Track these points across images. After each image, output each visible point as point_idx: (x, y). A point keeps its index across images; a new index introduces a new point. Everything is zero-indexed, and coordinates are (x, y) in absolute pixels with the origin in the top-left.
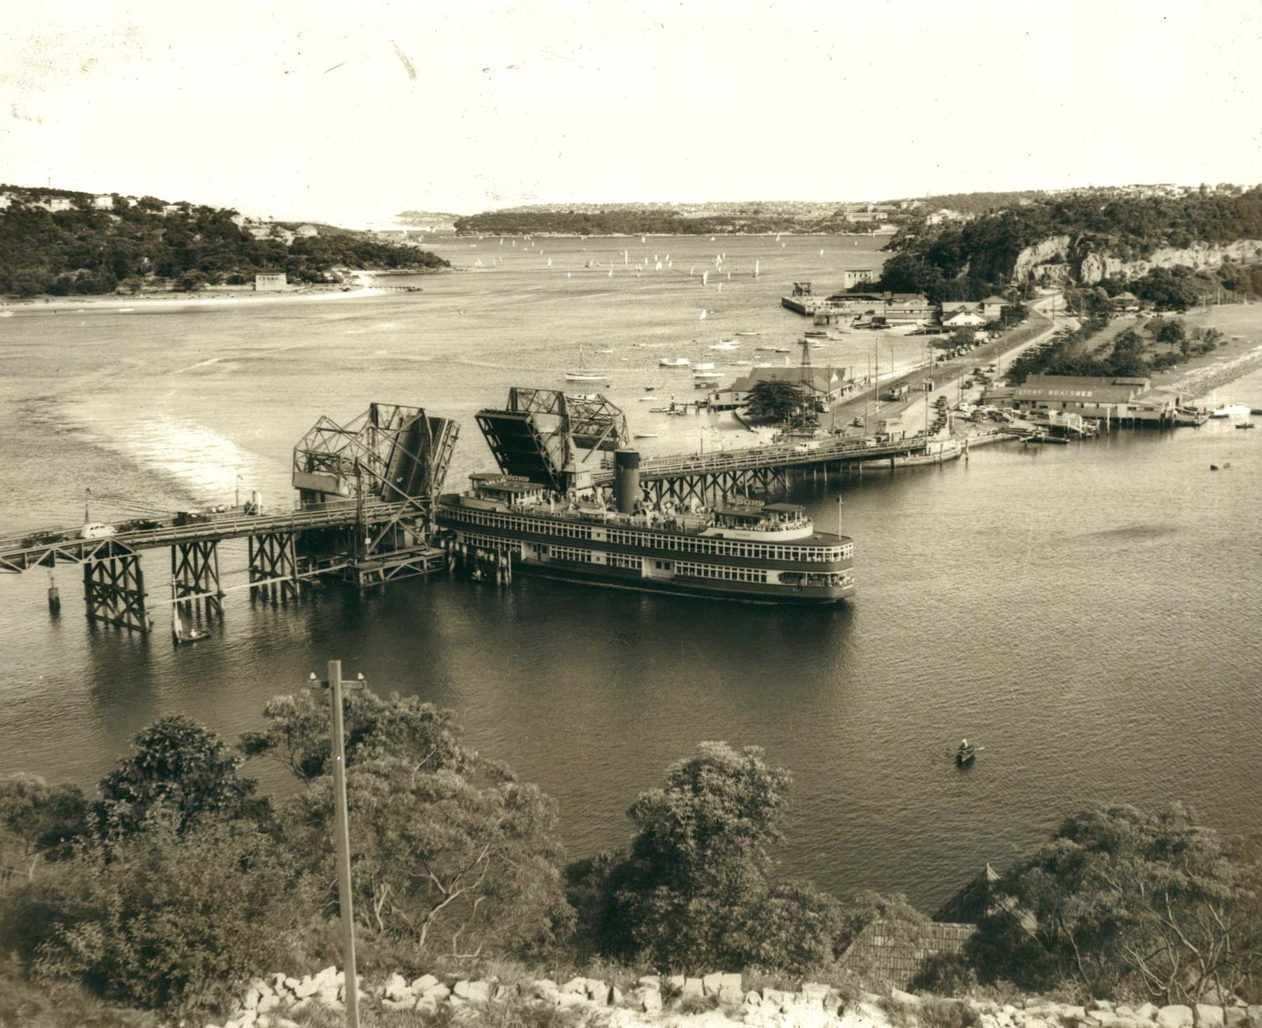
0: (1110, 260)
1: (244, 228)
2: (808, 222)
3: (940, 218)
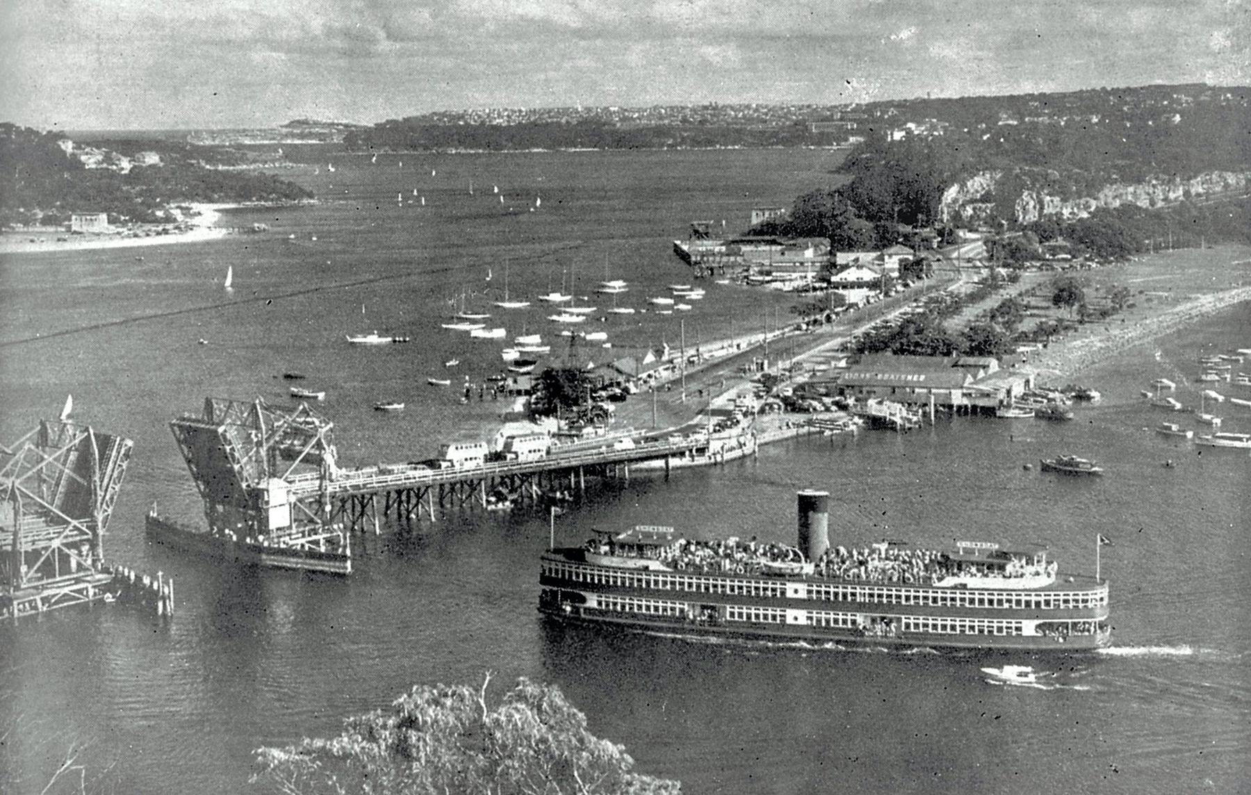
0: (1048, 198)
1: (73, 154)
2: (762, 133)
3: (903, 133)
